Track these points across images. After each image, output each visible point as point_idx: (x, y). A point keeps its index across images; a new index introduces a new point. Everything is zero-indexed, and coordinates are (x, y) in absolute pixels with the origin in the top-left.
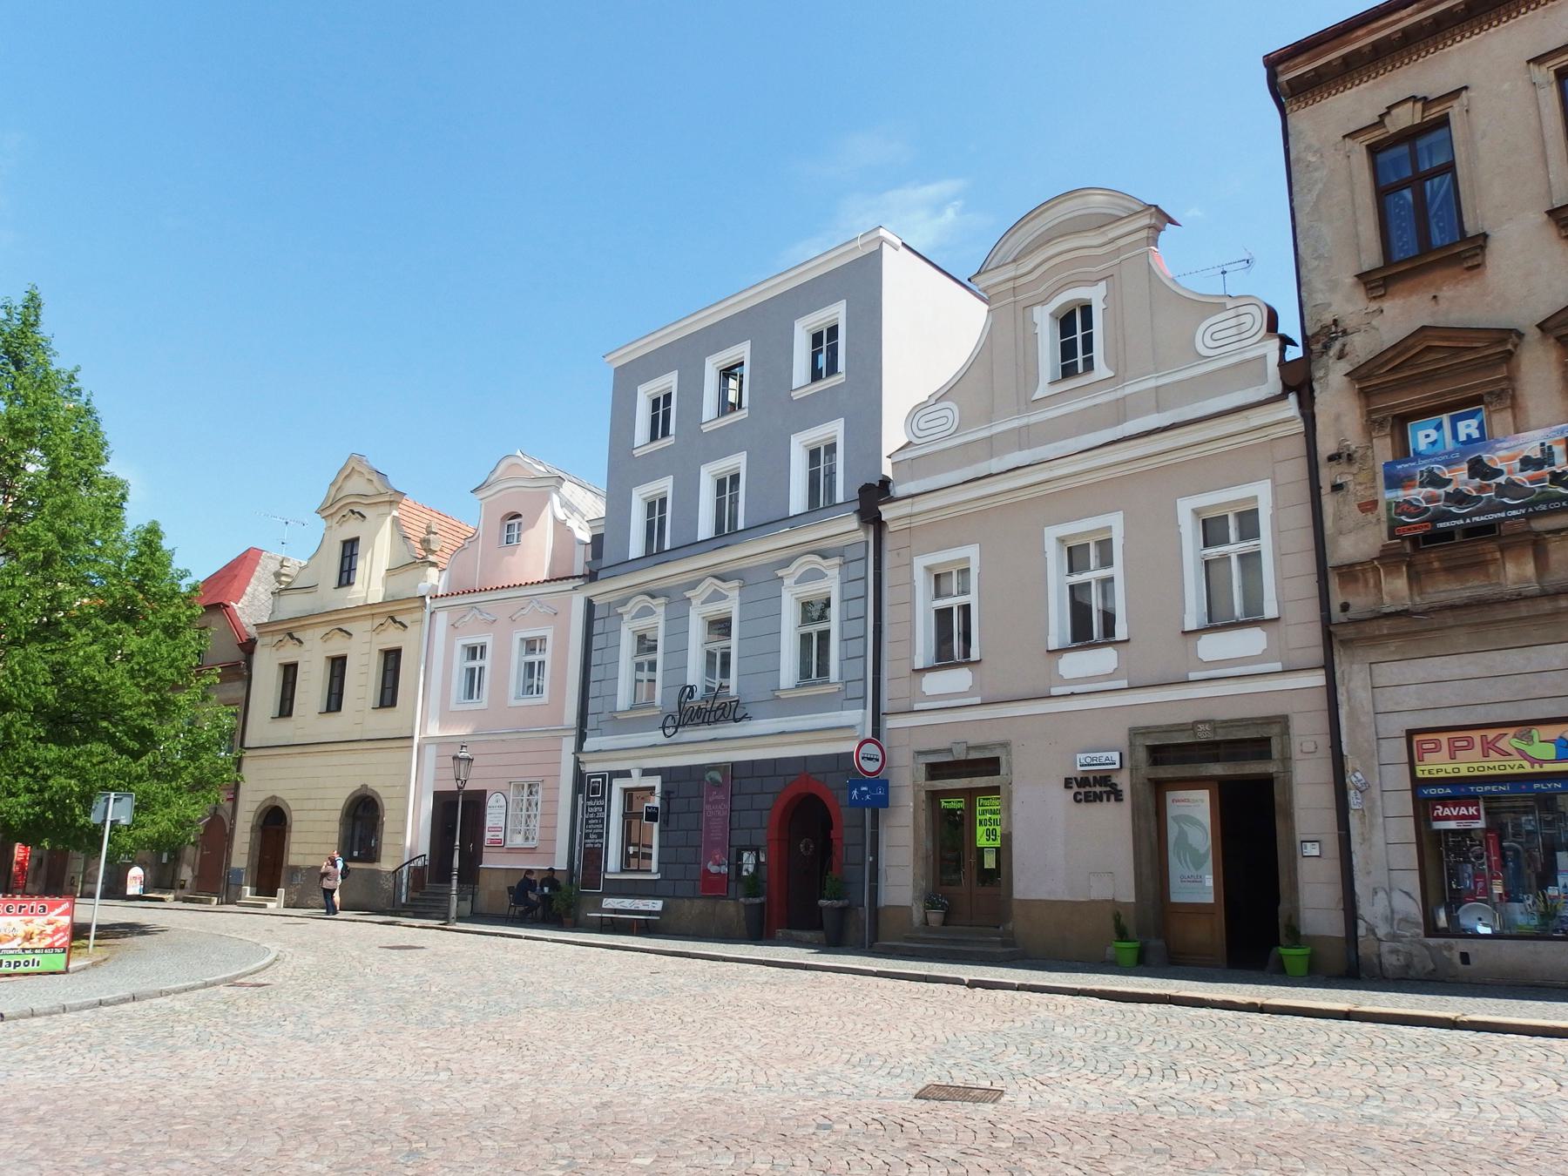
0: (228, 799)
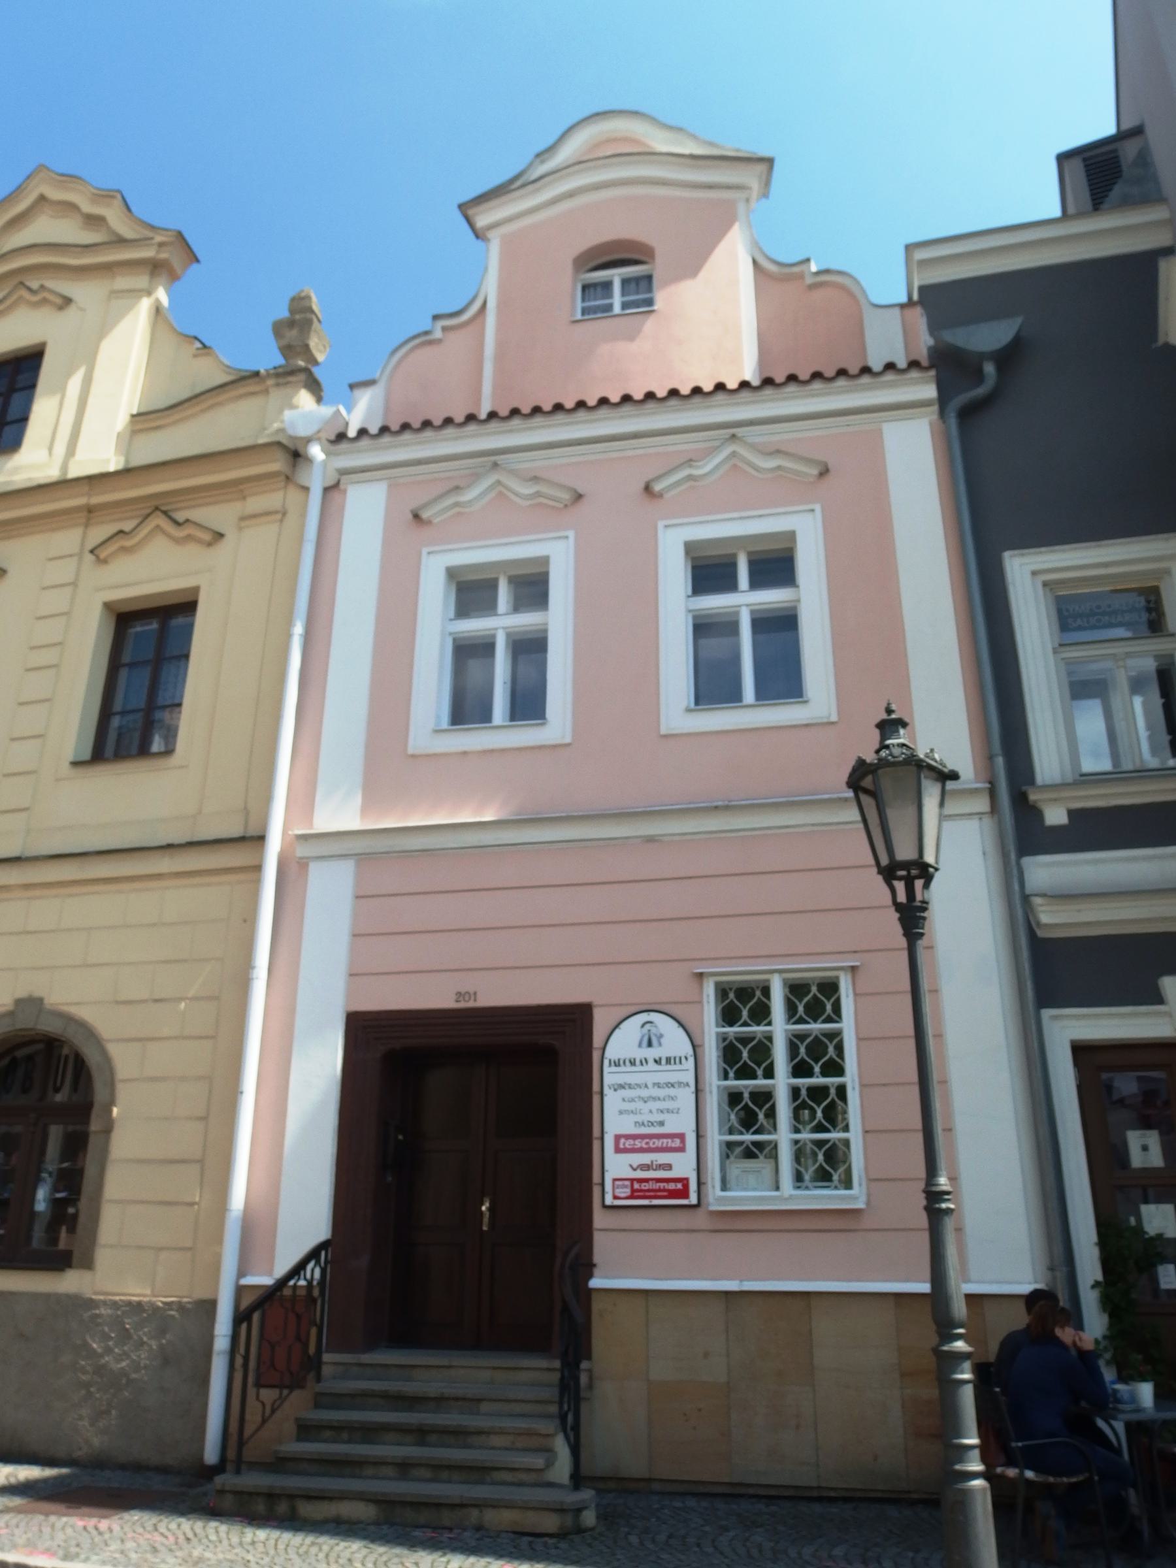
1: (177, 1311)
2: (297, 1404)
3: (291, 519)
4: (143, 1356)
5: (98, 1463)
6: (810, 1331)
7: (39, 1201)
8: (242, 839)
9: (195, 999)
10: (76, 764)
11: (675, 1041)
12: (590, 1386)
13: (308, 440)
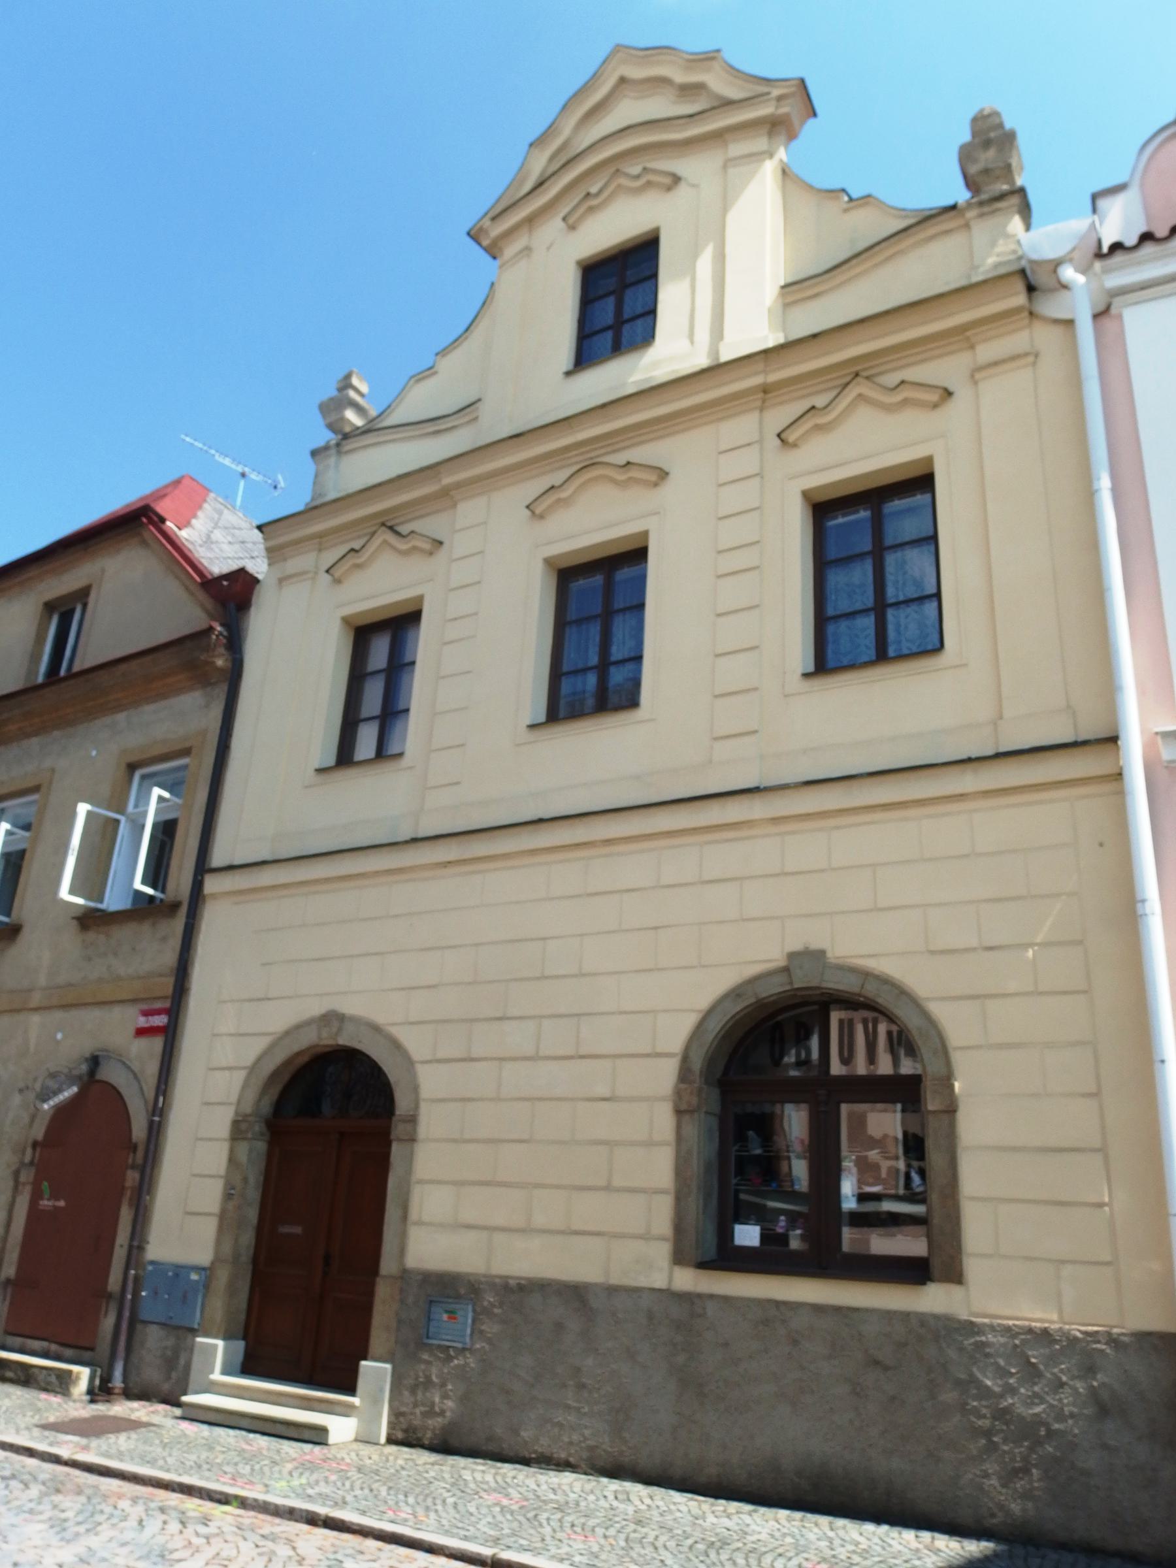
0: (141, 1032)
1: (1106, 1344)
4: (1065, 1401)
7: (847, 1197)
9: (1045, 945)
10: (806, 675)
13: (1056, 264)
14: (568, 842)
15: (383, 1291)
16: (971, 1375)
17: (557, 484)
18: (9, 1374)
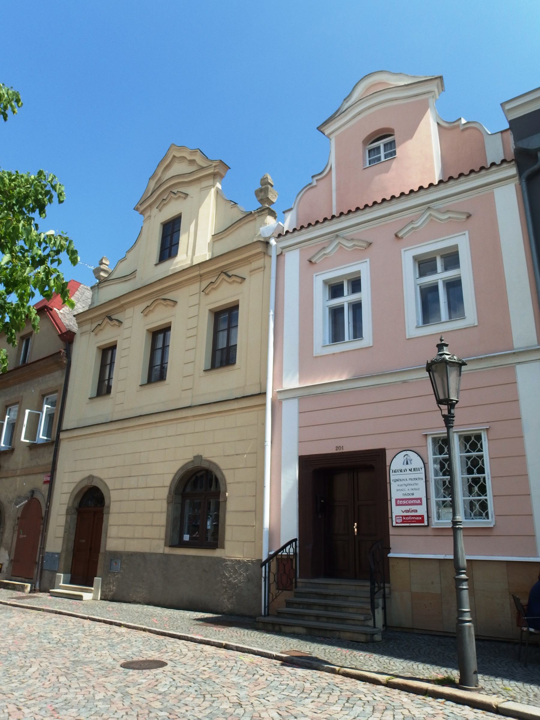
2: (287, 595)
3: (267, 270)
5: (231, 614)
6: (473, 575)
8: (259, 394)
10: (205, 371)
11: (417, 462)
12: (390, 593)
13: (270, 238)
14: (146, 423)
15: (101, 557)
16: (224, 573)
17: (149, 305)
18: (10, 587)
